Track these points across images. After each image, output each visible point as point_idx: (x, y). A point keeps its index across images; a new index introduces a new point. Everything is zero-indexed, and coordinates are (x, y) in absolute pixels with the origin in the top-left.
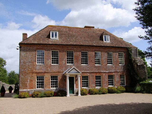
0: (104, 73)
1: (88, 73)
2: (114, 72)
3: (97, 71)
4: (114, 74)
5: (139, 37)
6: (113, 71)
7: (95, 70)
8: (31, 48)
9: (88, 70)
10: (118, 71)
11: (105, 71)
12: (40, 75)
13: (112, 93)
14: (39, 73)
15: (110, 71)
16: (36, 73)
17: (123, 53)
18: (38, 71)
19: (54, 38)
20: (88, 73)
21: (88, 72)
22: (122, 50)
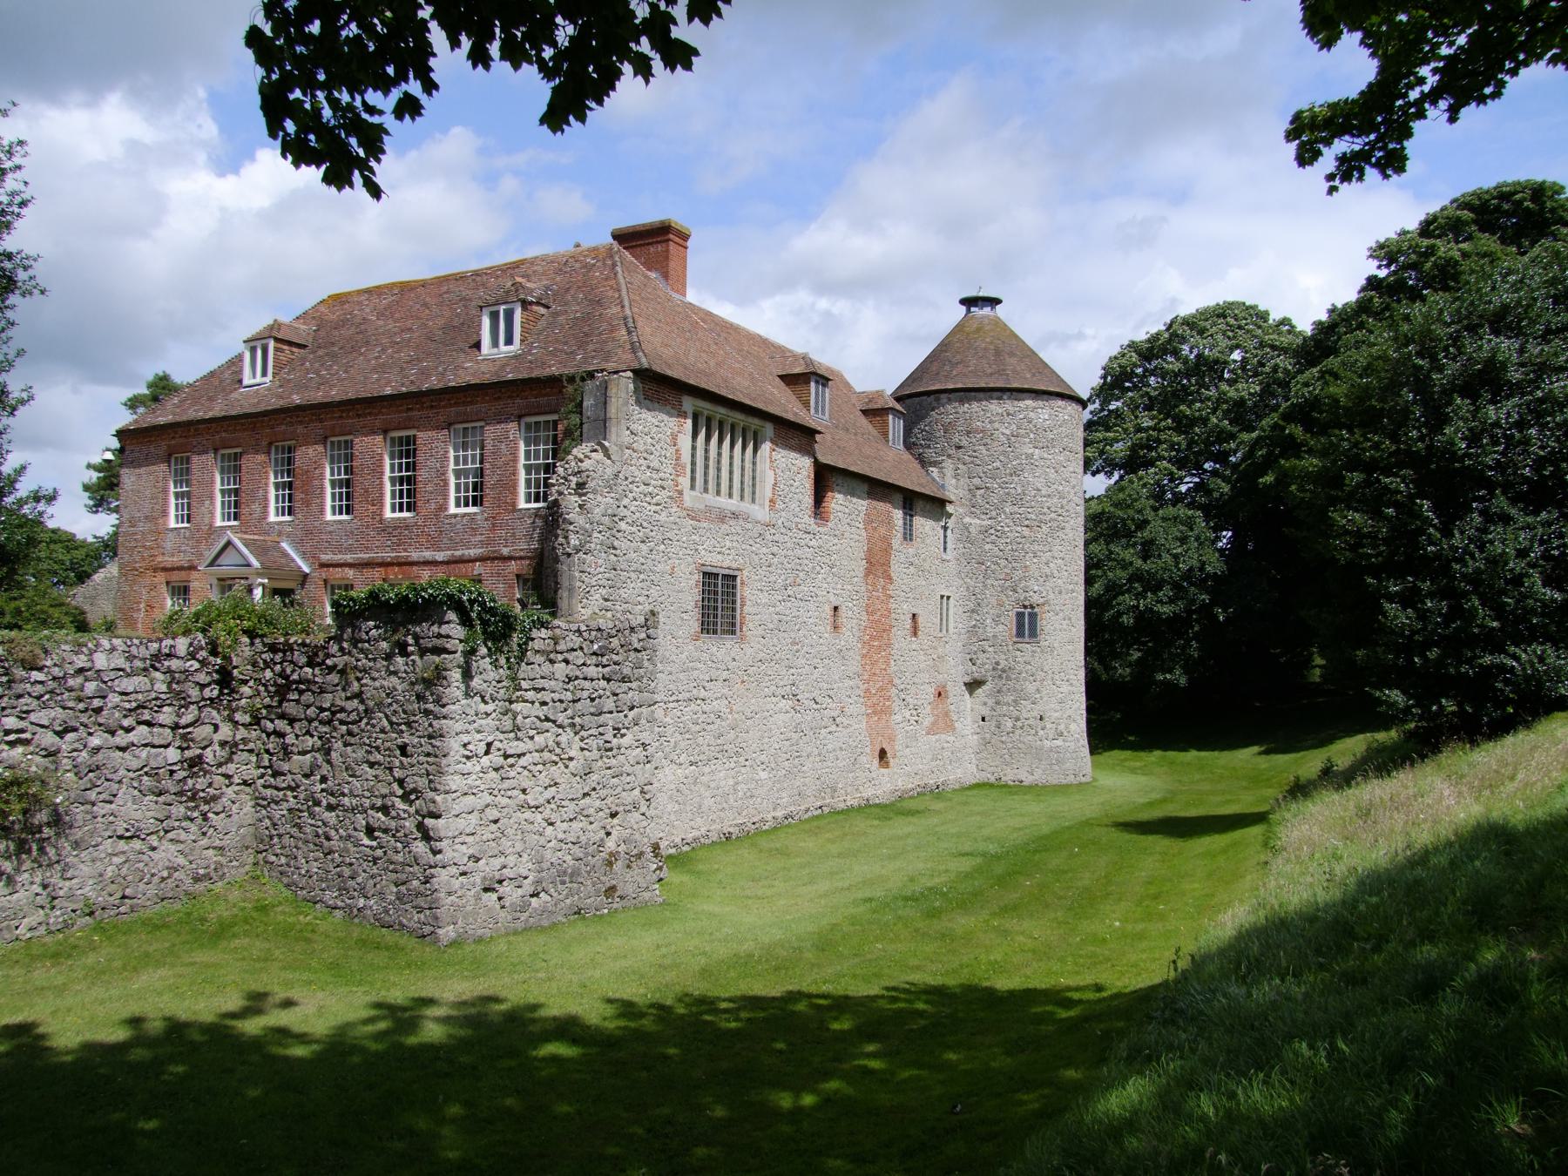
0: (427, 563)
1: (351, 565)
2: (482, 559)
3: (389, 555)
4: (478, 568)
5: (21, 143)
6: (473, 552)
7: (382, 547)
8: (152, 449)
9: (350, 550)
10: (505, 551)
11: (428, 555)
12: (176, 576)
13: (1501, 728)
14: (173, 569)
15: (458, 553)
16: (165, 569)
17: (1199, 513)
18: (170, 560)
19: (259, 379)
20: (351, 565)
21: (349, 558)
22: (543, 400)
